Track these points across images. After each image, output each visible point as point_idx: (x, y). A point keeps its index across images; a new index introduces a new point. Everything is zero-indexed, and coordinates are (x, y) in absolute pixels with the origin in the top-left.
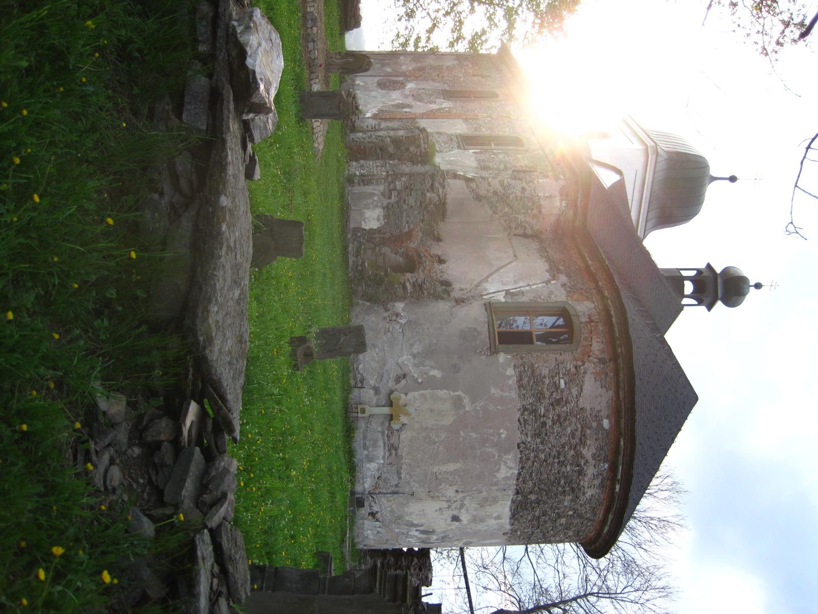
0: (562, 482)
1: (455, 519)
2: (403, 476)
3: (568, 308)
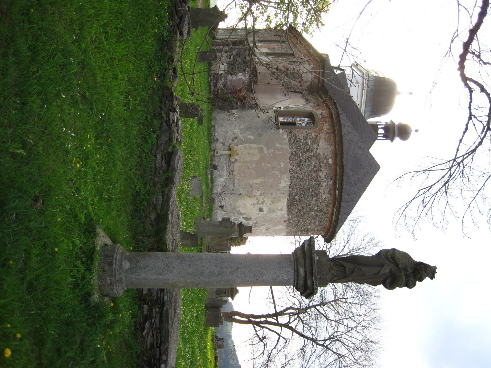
0: (311, 189)
1: (261, 210)
2: (235, 185)
3: (312, 112)
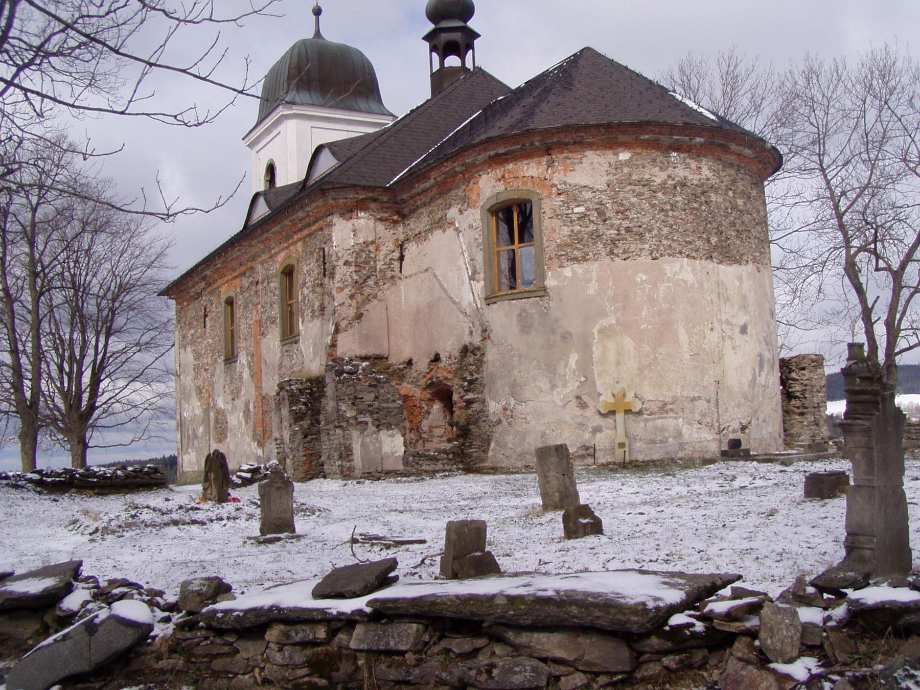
0: (695, 205)
